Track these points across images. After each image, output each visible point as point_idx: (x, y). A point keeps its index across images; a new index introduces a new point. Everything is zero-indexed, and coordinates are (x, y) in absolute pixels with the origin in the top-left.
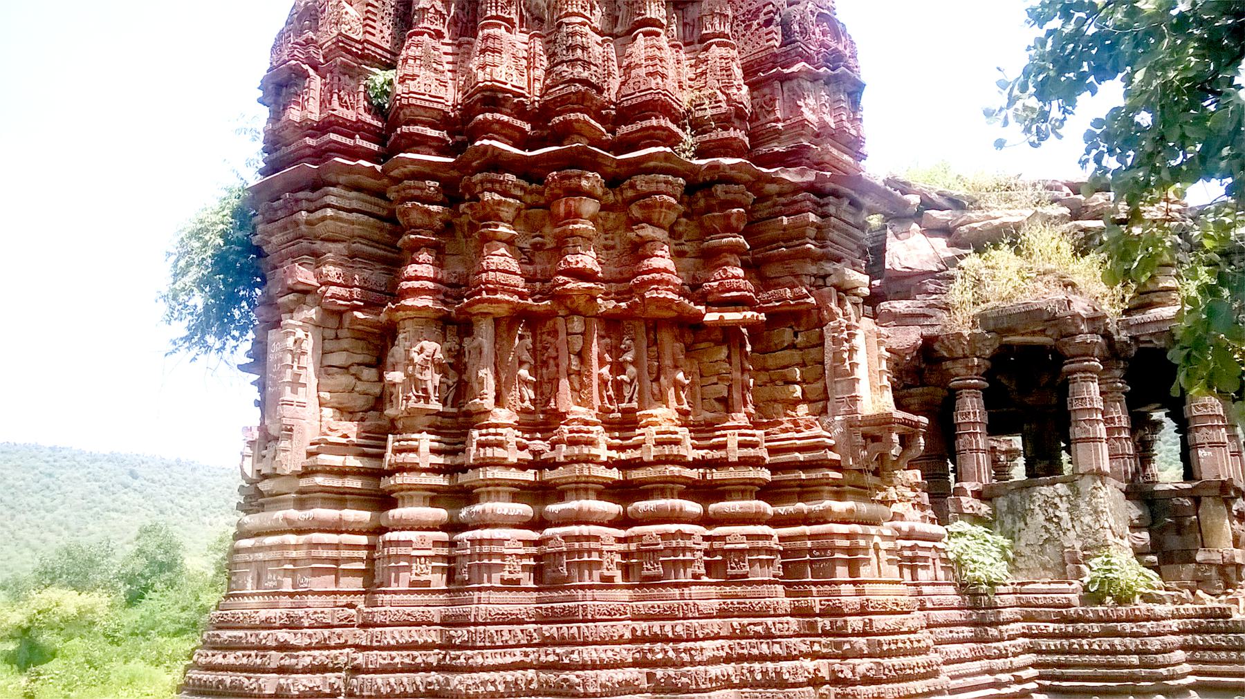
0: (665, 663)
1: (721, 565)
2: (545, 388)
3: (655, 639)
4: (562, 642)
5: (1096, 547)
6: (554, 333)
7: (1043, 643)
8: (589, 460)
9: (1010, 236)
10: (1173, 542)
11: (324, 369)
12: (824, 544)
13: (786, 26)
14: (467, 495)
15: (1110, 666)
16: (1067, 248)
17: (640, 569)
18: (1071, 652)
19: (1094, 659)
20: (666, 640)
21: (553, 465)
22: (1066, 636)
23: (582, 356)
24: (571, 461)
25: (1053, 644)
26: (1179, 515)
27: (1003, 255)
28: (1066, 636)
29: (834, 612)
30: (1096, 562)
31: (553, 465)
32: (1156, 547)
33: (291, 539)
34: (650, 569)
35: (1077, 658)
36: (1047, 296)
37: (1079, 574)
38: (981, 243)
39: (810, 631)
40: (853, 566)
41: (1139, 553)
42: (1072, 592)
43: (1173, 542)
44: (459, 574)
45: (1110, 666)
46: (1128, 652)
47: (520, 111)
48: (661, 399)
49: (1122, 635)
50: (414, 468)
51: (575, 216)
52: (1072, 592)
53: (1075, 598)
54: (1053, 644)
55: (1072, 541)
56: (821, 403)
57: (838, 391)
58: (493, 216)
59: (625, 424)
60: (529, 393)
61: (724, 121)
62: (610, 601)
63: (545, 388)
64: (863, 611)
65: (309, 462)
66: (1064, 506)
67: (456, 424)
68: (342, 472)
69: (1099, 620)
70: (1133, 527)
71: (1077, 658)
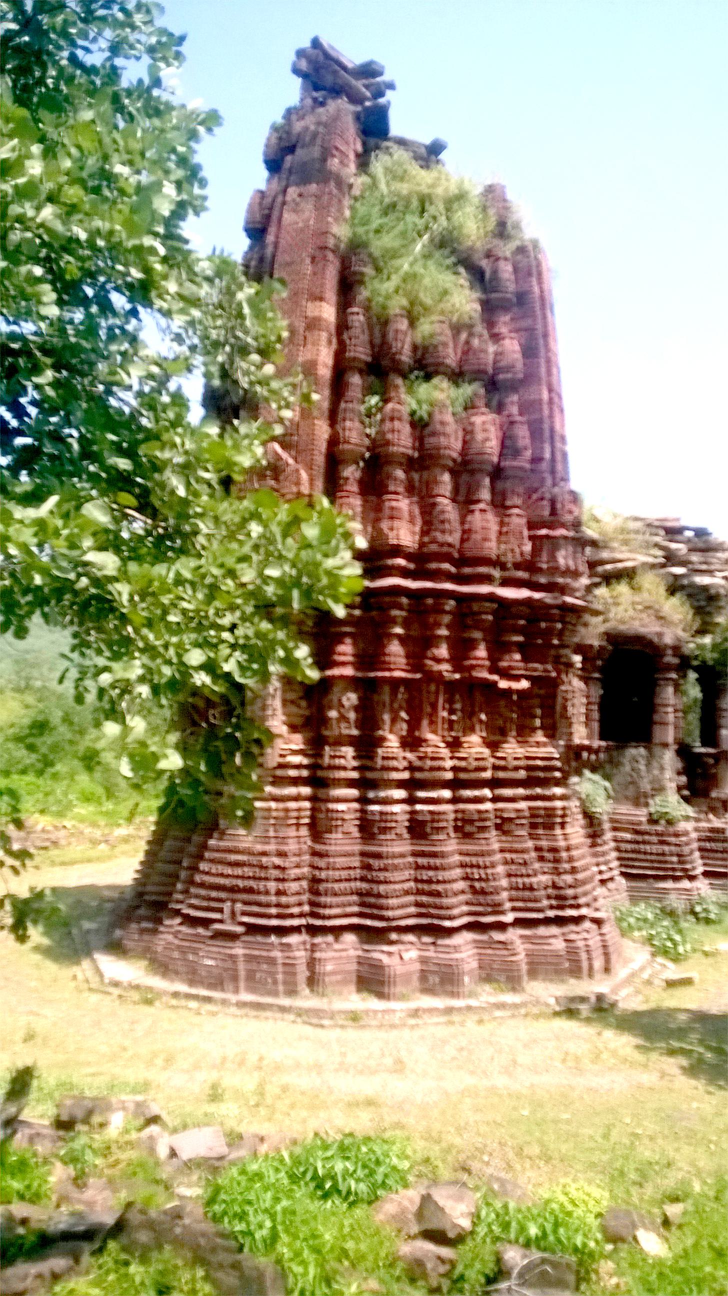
0: (480, 879)
1: (503, 825)
2: (414, 724)
3: (472, 866)
4: (429, 868)
5: (660, 789)
6: (421, 691)
7: (624, 846)
8: (440, 769)
9: (628, 575)
10: (700, 784)
11: (285, 702)
12: (550, 813)
13: (553, 502)
14: (374, 785)
15: (660, 862)
16: (662, 591)
17: (466, 828)
18: (639, 852)
19: (653, 858)
20: (479, 867)
21: (421, 769)
22: (638, 842)
23: (434, 706)
24: (432, 769)
25: (629, 847)
26: (706, 766)
27: (622, 588)
28: (638, 842)
29: (554, 850)
30: (658, 799)
31: (421, 769)
32: (688, 787)
33: (273, 805)
34: (468, 828)
35: (642, 857)
36: (648, 627)
37: (647, 805)
38: (609, 579)
39: (541, 859)
40: (563, 825)
41: (679, 789)
42: (641, 815)
43: (700, 784)
44: (369, 828)
45: (660, 862)
46: (672, 855)
47: (409, 557)
48: (472, 730)
49: (668, 844)
50: (344, 768)
51: (438, 625)
52: (641, 815)
53: (644, 819)
54: (629, 847)
55: (645, 786)
56: (552, 732)
57: (562, 729)
58: (393, 621)
59: (455, 745)
60: (405, 726)
61: (517, 566)
62: (450, 845)
63: (414, 724)
64: (568, 849)
65: (281, 760)
66: (643, 762)
67: (366, 745)
68: (298, 767)
69: (657, 834)
70: (679, 773)
71: (642, 857)
